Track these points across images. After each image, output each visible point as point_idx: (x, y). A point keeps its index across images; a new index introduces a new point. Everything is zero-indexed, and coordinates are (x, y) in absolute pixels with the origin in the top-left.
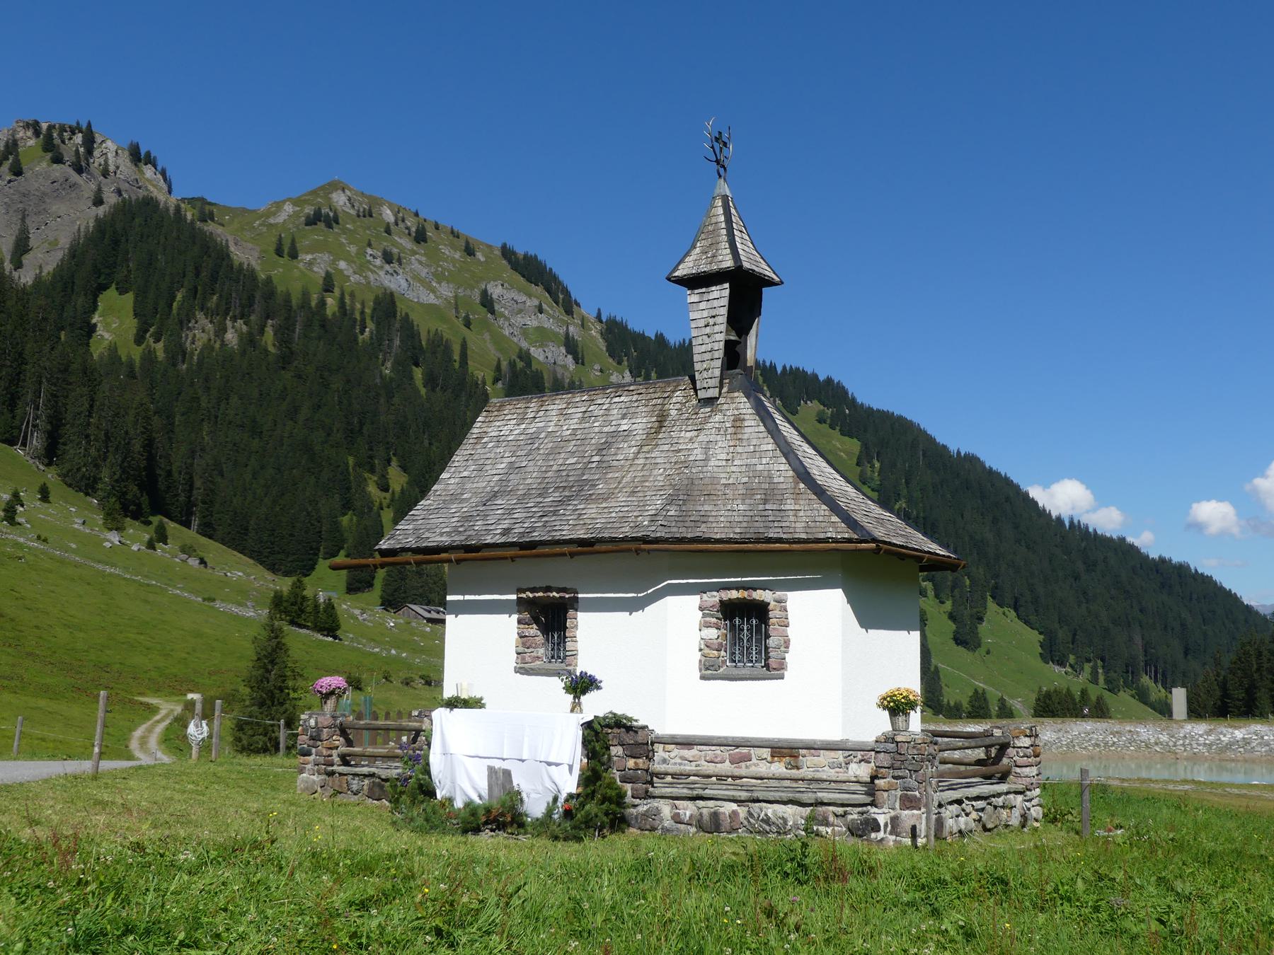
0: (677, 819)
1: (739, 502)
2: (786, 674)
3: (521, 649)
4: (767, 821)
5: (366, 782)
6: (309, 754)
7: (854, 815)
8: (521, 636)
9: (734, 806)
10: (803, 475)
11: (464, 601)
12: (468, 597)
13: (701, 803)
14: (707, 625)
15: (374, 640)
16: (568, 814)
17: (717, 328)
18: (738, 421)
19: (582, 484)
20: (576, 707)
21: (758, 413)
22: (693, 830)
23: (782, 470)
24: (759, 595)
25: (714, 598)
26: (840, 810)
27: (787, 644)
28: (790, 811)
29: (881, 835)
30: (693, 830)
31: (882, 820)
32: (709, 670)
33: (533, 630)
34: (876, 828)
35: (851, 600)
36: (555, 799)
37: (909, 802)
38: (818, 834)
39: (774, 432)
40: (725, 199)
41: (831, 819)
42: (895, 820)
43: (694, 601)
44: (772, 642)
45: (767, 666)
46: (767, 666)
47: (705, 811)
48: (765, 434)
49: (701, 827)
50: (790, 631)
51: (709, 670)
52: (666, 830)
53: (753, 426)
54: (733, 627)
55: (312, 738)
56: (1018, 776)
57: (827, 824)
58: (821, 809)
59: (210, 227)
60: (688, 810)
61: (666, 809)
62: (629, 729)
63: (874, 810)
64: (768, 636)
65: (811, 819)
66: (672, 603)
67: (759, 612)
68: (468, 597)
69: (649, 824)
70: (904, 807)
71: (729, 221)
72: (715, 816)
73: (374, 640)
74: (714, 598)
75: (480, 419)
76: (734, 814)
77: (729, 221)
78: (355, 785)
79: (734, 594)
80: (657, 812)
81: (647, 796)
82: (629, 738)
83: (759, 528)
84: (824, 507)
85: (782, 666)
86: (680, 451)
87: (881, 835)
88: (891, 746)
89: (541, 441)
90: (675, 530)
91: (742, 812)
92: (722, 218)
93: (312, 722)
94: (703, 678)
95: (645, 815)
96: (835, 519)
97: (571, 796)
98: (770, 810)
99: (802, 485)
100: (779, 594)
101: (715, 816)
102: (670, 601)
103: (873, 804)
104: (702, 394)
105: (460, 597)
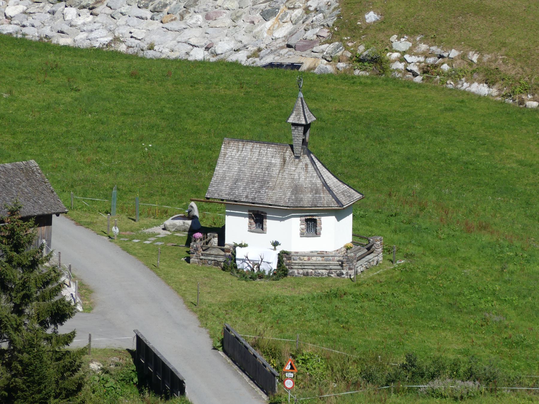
0: (298, 273)
1: (309, 194)
2: (321, 236)
3: (250, 225)
4: (319, 273)
5: (213, 262)
6: (194, 254)
7: (338, 272)
8: (250, 222)
9: (312, 270)
10: (325, 184)
11: (230, 212)
12: (231, 211)
13: (304, 270)
14: (302, 224)
15: (362, 198)
16: (274, 274)
17: (300, 138)
18: (306, 165)
19: (265, 181)
20: (275, 249)
21: (312, 163)
22: (302, 276)
23: (319, 182)
24: (315, 218)
25: (304, 218)
26: (335, 271)
27: (321, 229)
28: (324, 271)
29: (344, 276)
30: (302, 276)
31: (344, 273)
32: (302, 235)
33: (252, 221)
34: (343, 274)
35: (336, 217)
36: (271, 270)
37: (350, 269)
38: (330, 276)
39: (316, 169)
40: (301, 98)
41: (333, 273)
42: (347, 273)
43: (299, 219)
44: (318, 228)
45: (316, 234)
46: (316, 234)
47: (305, 272)
48: (314, 170)
49: (304, 275)
50: (322, 225)
51: (302, 235)
52: (296, 276)
53: (311, 167)
54: (308, 224)
55: (195, 250)
56: (376, 251)
57: (332, 274)
58: (331, 271)
59: (26, 37)
60: (301, 271)
61: (296, 271)
62: (287, 254)
63: (342, 270)
64: (316, 227)
65: (329, 273)
66: (293, 219)
67: (315, 221)
68: (231, 211)
69: (292, 275)
70: (349, 270)
71: (303, 107)
72: (307, 272)
73: (362, 198)
74: (304, 218)
75: (222, 146)
76: (312, 272)
77: (303, 107)
78: (209, 262)
79: (308, 217)
80: (294, 272)
81: (292, 268)
82: (287, 256)
83: (297, 204)
84: (331, 196)
85: (320, 234)
86: (291, 174)
87: (344, 276)
88: (347, 257)
89: (247, 161)
90: (295, 204)
91: (313, 271)
92: (301, 105)
93: (195, 246)
94: (301, 237)
95: (291, 273)
96: (333, 200)
97: (275, 270)
98: (320, 271)
99: (324, 188)
100: (319, 217)
101: (307, 272)
102: (293, 219)
103: (342, 269)
104: (295, 155)
105: (229, 211)
